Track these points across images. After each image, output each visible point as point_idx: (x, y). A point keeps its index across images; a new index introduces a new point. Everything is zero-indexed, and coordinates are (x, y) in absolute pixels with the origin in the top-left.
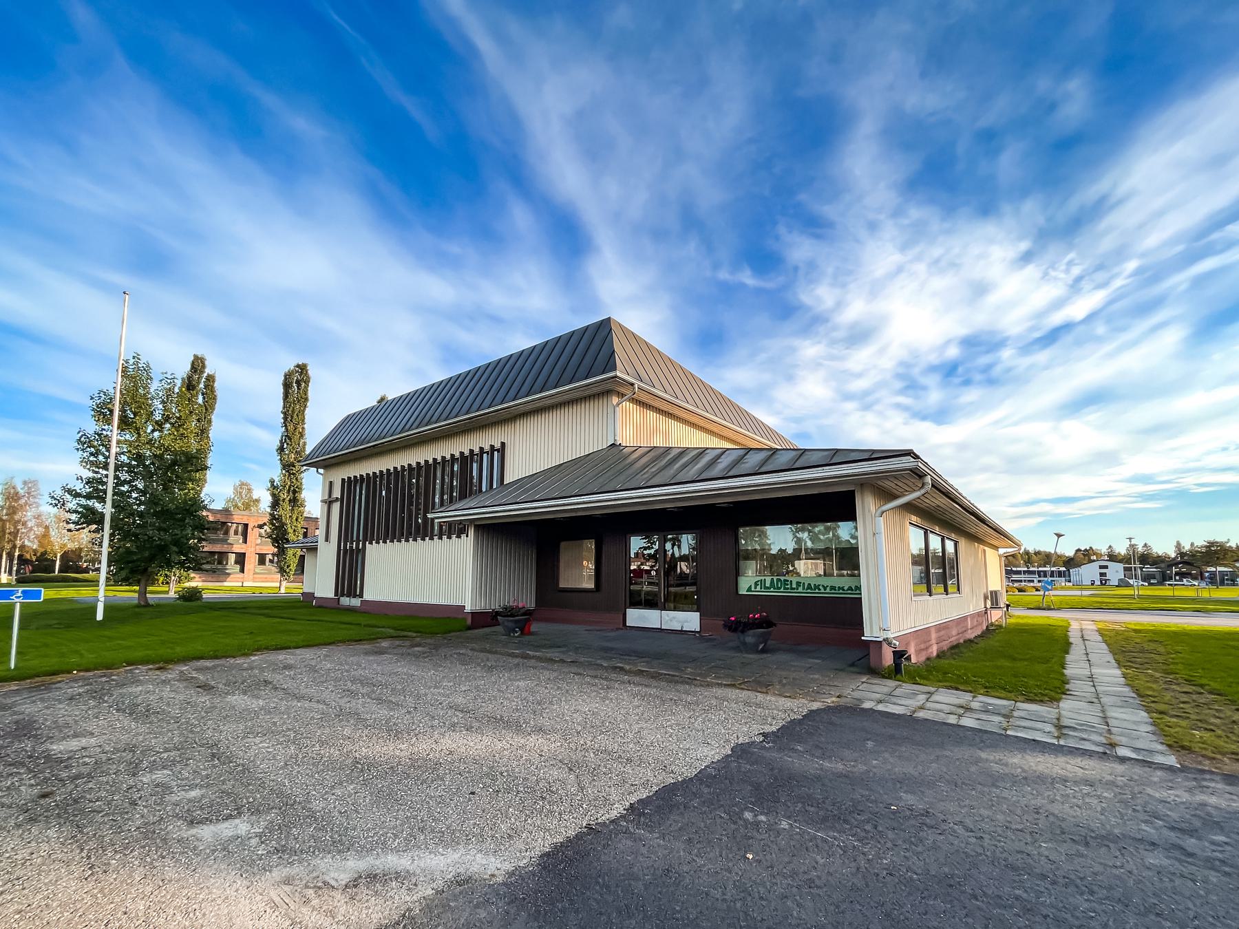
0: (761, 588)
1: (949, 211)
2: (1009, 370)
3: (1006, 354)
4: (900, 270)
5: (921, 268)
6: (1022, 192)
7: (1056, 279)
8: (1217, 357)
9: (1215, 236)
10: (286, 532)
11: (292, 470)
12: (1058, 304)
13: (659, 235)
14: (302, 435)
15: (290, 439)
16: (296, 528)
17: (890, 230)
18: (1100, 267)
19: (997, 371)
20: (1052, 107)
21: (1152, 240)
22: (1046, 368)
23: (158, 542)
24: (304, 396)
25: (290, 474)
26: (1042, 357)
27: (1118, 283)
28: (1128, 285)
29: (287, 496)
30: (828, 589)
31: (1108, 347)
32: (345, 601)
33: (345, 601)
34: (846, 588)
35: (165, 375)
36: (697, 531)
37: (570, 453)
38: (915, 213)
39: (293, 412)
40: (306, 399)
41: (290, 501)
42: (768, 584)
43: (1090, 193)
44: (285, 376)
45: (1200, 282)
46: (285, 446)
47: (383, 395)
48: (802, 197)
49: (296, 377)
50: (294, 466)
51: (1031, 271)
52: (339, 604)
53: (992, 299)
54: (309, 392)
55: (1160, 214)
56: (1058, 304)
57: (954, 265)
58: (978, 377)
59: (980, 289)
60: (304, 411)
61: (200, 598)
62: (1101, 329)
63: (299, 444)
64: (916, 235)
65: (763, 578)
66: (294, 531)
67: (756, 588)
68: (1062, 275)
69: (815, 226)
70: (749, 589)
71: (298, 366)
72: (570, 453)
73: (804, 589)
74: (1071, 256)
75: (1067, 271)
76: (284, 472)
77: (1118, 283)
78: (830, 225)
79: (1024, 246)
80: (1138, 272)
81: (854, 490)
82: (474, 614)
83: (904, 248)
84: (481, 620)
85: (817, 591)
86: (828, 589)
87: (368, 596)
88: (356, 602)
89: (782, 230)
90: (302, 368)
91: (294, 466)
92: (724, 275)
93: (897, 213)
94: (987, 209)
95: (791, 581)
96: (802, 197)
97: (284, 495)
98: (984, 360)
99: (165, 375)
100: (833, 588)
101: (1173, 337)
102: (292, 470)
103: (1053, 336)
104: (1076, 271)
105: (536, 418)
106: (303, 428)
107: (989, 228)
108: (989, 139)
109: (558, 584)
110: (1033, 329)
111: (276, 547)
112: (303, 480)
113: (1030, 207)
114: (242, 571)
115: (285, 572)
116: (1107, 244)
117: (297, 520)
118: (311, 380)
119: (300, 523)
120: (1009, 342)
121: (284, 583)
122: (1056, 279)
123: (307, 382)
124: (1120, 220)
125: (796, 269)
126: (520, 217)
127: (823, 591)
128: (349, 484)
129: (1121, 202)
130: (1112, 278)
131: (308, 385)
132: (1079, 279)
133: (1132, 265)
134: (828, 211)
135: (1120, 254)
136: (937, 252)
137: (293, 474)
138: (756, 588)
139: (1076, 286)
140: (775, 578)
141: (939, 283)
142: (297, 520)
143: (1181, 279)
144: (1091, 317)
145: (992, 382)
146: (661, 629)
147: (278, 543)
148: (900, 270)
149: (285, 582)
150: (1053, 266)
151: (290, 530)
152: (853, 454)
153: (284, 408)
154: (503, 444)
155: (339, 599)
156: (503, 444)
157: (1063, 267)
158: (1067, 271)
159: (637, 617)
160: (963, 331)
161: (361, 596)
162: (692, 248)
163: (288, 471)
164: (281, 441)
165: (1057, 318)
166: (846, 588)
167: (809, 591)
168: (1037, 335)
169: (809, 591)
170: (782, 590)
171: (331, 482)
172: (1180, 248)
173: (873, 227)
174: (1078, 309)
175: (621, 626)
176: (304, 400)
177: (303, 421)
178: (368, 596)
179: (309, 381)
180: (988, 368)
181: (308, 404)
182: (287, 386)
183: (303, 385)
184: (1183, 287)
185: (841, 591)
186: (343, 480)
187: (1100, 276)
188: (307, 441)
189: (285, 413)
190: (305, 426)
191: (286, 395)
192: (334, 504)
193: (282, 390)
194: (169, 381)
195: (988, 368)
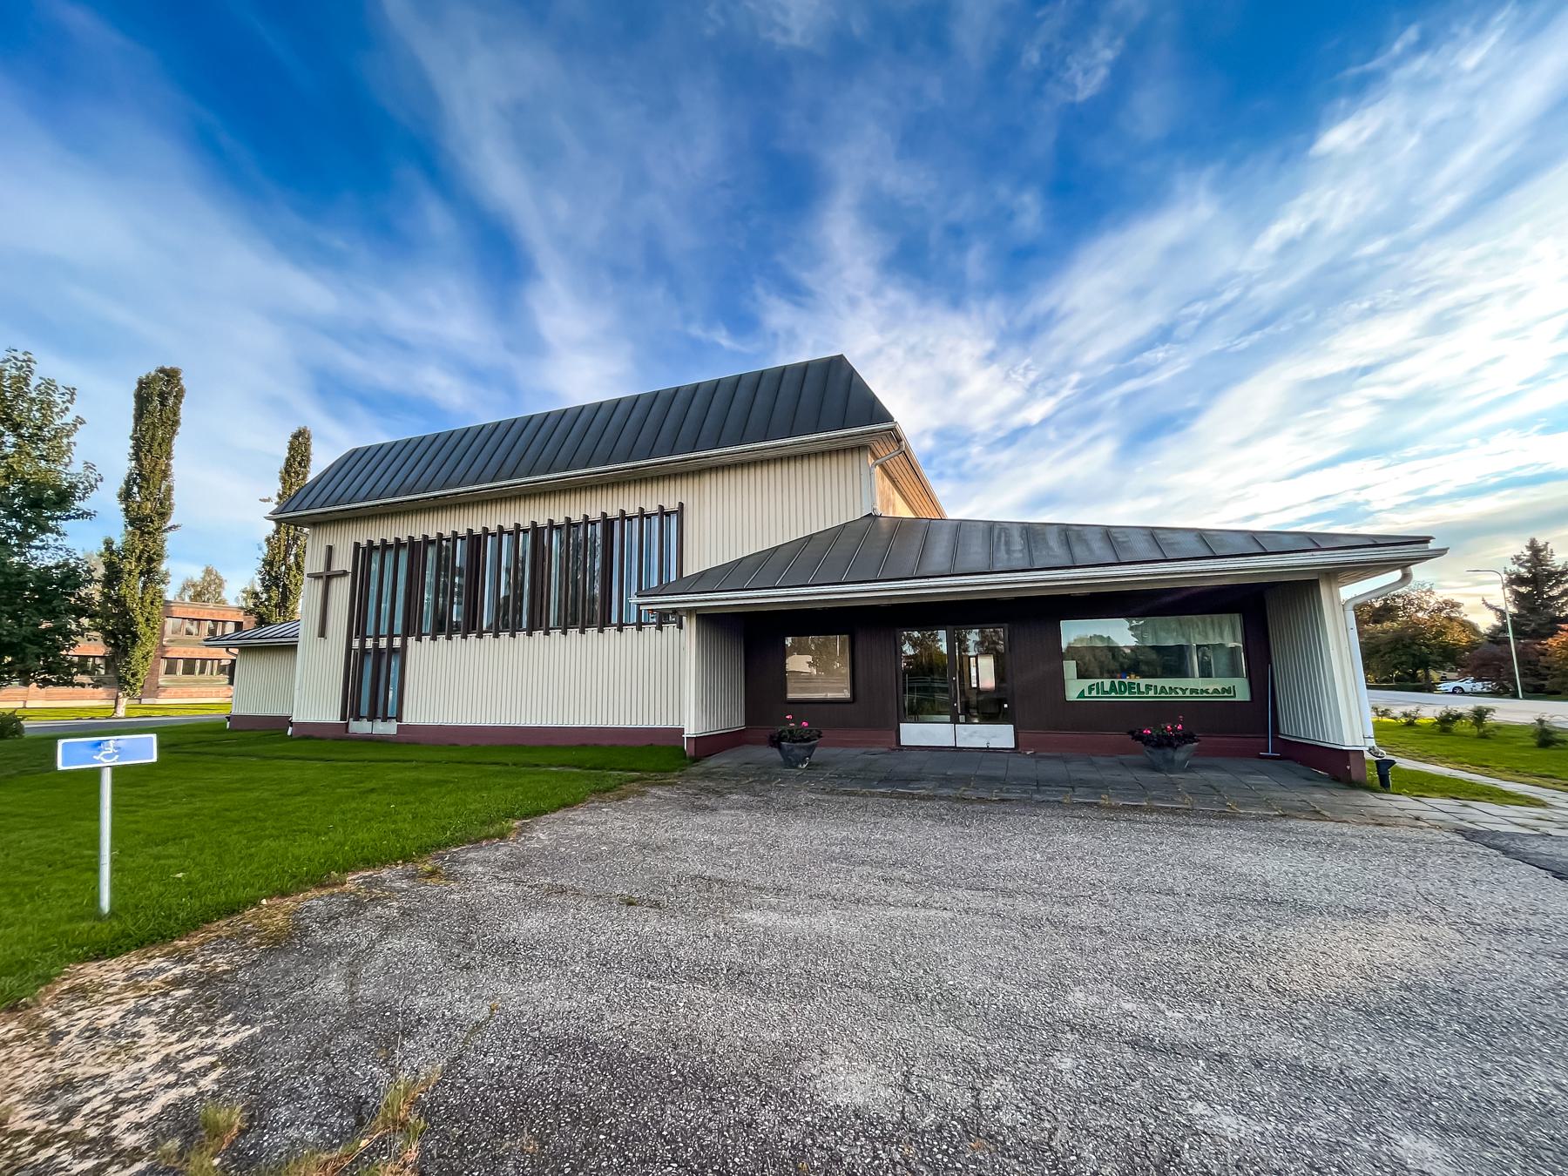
0: (1098, 693)
1: (924, 299)
2: (977, 466)
3: (975, 450)
4: (879, 351)
5: (898, 353)
6: (987, 291)
7: (1016, 382)
8: (1139, 470)
9: (1136, 360)
10: (132, 622)
11: (148, 526)
12: (1018, 406)
13: (619, 272)
14: (165, 474)
15: (147, 481)
16: (150, 617)
17: (869, 309)
18: (1050, 376)
19: (967, 466)
20: (1011, 216)
21: (1090, 357)
22: (1008, 467)
23: (7, 639)
24: (171, 416)
25: (143, 533)
26: (1005, 456)
27: (1065, 393)
28: (1074, 394)
29: (136, 567)
30: (1188, 693)
31: (1058, 453)
32: (361, 727)
33: (361, 727)
34: (1210, 691)
35: (14, 354)
36: (1006, 625)
37: (793, 527)
38: (893, 295)
39: (153, 438)
40: (176, 423)
41: (141, 573)
42: (1107, 688)
43: (1043, 303)
44: (140, 382)
45: (1128, 399)
46: (135, 489)
47: (302, 426)
48: (781, 258)
49: (160, 386)
50: (152, 521)
51: (995, 370)
52: (347, 731)
53: (963, 393)
54: (181, 411)
55: (1096, 333)
56: (1018, 406)
57: (929, 356)
58: (950, 471)
59: (952, 383)
60: (171, 439)
61: (19, 730)
62: (1051, 434)
63: (160, 489)
64: (895, 316)
65: (1100, 681)
66: (148, 620)
67: (1090, 693)
68: (1021, 379)
69: (794, 292)
70: (1082, 694)
71: (162, 371)
72: (793, 527)
73: (1156, 693)
74: (1028, 361)
75: (1024, 375)
76: (130, 528)
77: (1065, 393)
78: (809, 293)
79: (989, 345)
80: (1080, 384)
81: (1317, 580)
82: (698, 741)
83: (882, 330)
84: (708, 746)
85: (1173, 695)
86: (1188, 693)
87: (409, 718)
88: (390, 728)
89: (759, 290)
90: (171, 376)
91: (152, 521)
92: (696, 330)
93: (876, 293)
94: (956, 303)
95: (1139, 684)
96: (781, 258)
97: (129, 565)
98: (955, 454)
99: (14, 354)
100: (1192, 691)
101: (1106, 450)
102: (148, 526)
103: (1015, 436)
104: (1032, 376)
105: (745, 476)
106: (168, 465)
107: (958, 323)
108: (957, 234)
109: (784, 691)
110: (998, 427)
111: (111, 645)
112: (166, 543)
113: (994, 307)
114: (231, 682)
115: (128, 683)
116: (1055, 355)
117: (152, 603)
118: (186, 395)
119: (157, 607)
120: (976, 439)
121: (124, 702)
122: (1016, 382)
123: (179, 396)
124: (1067, 332)
125: (775, 335)
126: (437, 219)
127: (1181, 694)
128: (364, 554)
129: (1065, 317)
130: (1062, 386)
131: (181, 402)
132: (1034, 385)
133: (1075, 378)
134: (807, 278)
135: (1066, 366)
136: (913, 339)
137: (149, 533)
138: (1090, 693)
139: (1032, 390)
140: (1116, 681)
141: (916, 371)
142: (152, 603)
143: (1112, 395)
144: (1044, 422)
145: (963, 477)
146: (956, 749)
147: (116, 639)
148: (879, 351)
149: (126, 700)
150: (1013, 368)
151: (140, 619)
152: (1342, 539)
153: (135, 431)
154: (681, 505)
155: (347, 724)
156: (681, 505)
157: (1021, 371)
158: (1024, 375)
159: (913, 733)
160: (936, 423)
161: (399, 718)
162: (658, 293)
163: (139, 529)
164: (127, 483)
165: (1018, 420)
166: (1210, 691)
167: (1163, 695)
168: (1000, 434)
169: (1163, 695)
170: (1127, 694)
171: (330, 549)
172: (1110, 368)
173: (853, 303)
174: (1036, 412)
175: (894, 746)
176: (172, 423)
177: (169, 454)
178: (409, 718)
179: (182, 396)
180: (959, 463)
181: (179, 430)
182: (142, 399)
183: (171, 401)
184: (1115, 403)
185: (1205, 694)
186: (357, 545)
187: (1051, 384)
188: (176, 485)
189: (136, 440)
190: (172, 462)
191: (139, 417)
192: (335, 579)
193: (134, 404)
194: (19, 364)
195: (959, 463)
